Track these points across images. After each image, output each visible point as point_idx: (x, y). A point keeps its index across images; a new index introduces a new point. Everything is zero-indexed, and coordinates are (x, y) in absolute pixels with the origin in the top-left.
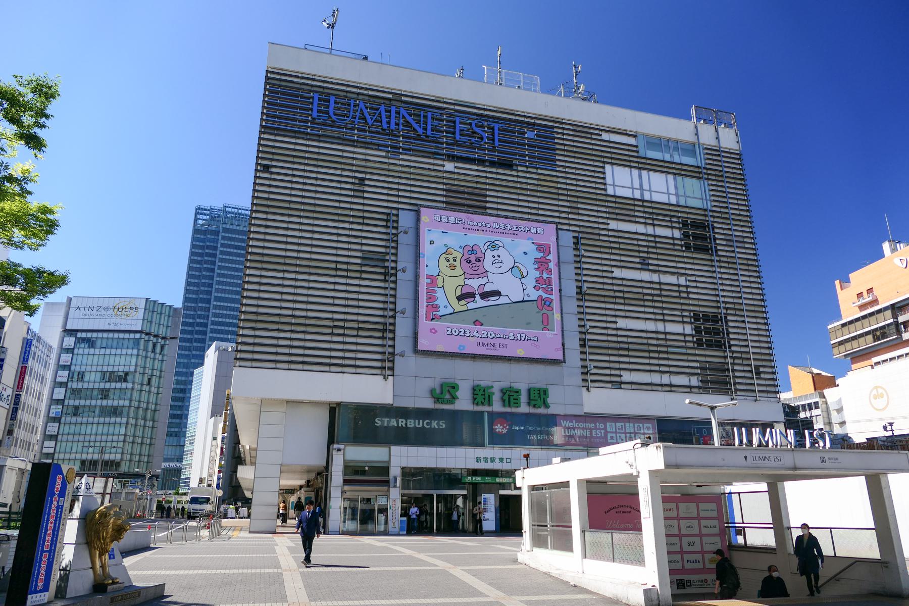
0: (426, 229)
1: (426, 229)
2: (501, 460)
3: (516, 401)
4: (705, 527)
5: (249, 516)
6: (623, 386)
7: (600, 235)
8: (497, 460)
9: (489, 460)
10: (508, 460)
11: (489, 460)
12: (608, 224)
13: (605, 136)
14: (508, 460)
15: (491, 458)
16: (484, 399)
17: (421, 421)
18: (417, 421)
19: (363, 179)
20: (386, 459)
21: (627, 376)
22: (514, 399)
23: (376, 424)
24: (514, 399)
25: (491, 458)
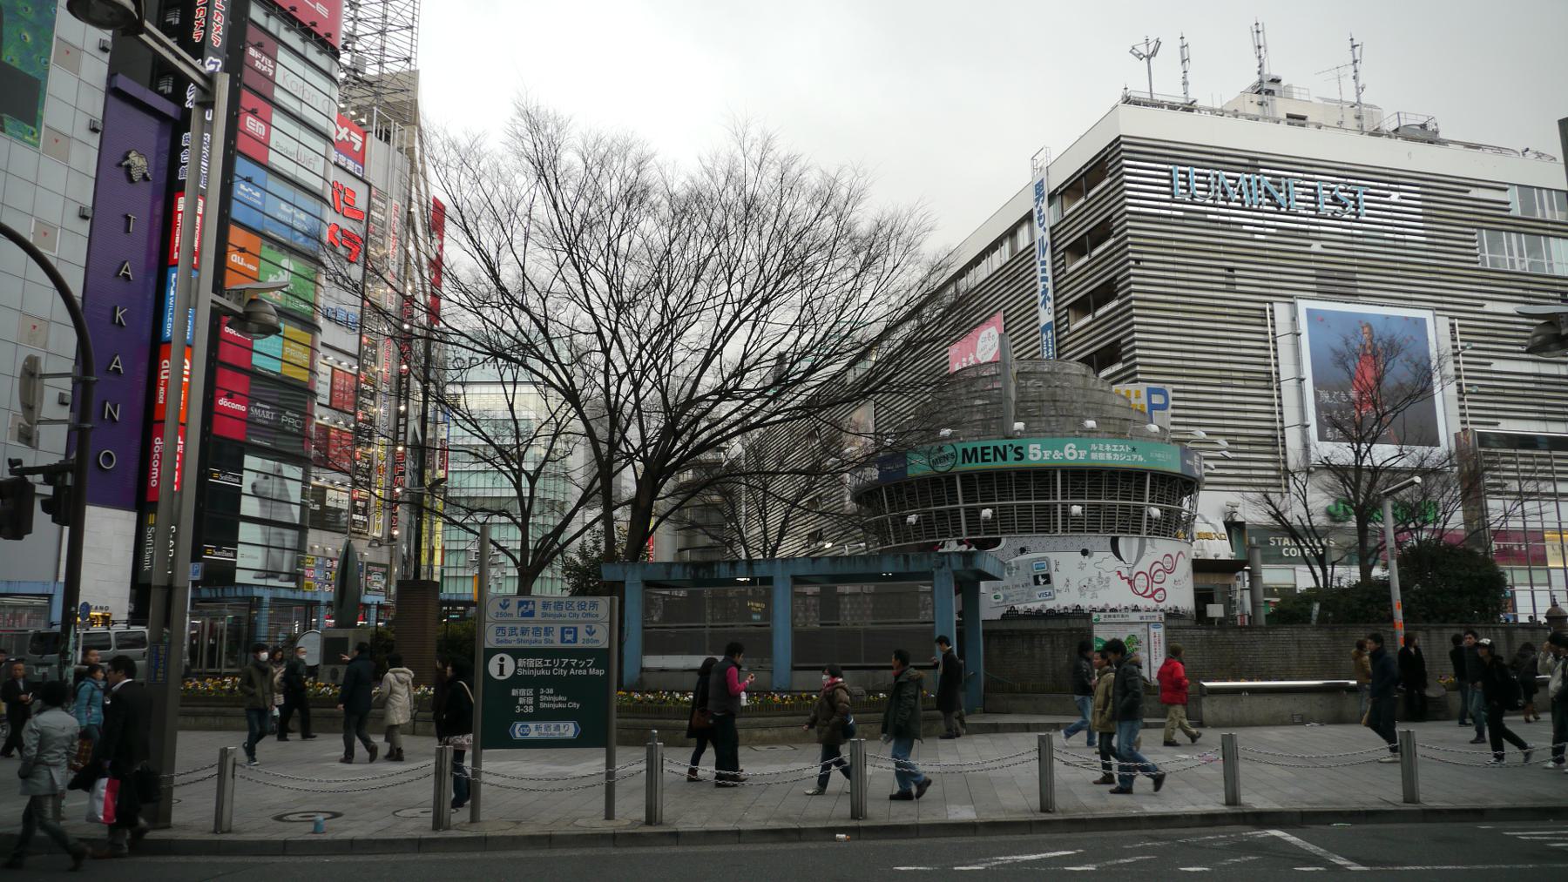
13: (1474, 193)
20: (1293, 582)
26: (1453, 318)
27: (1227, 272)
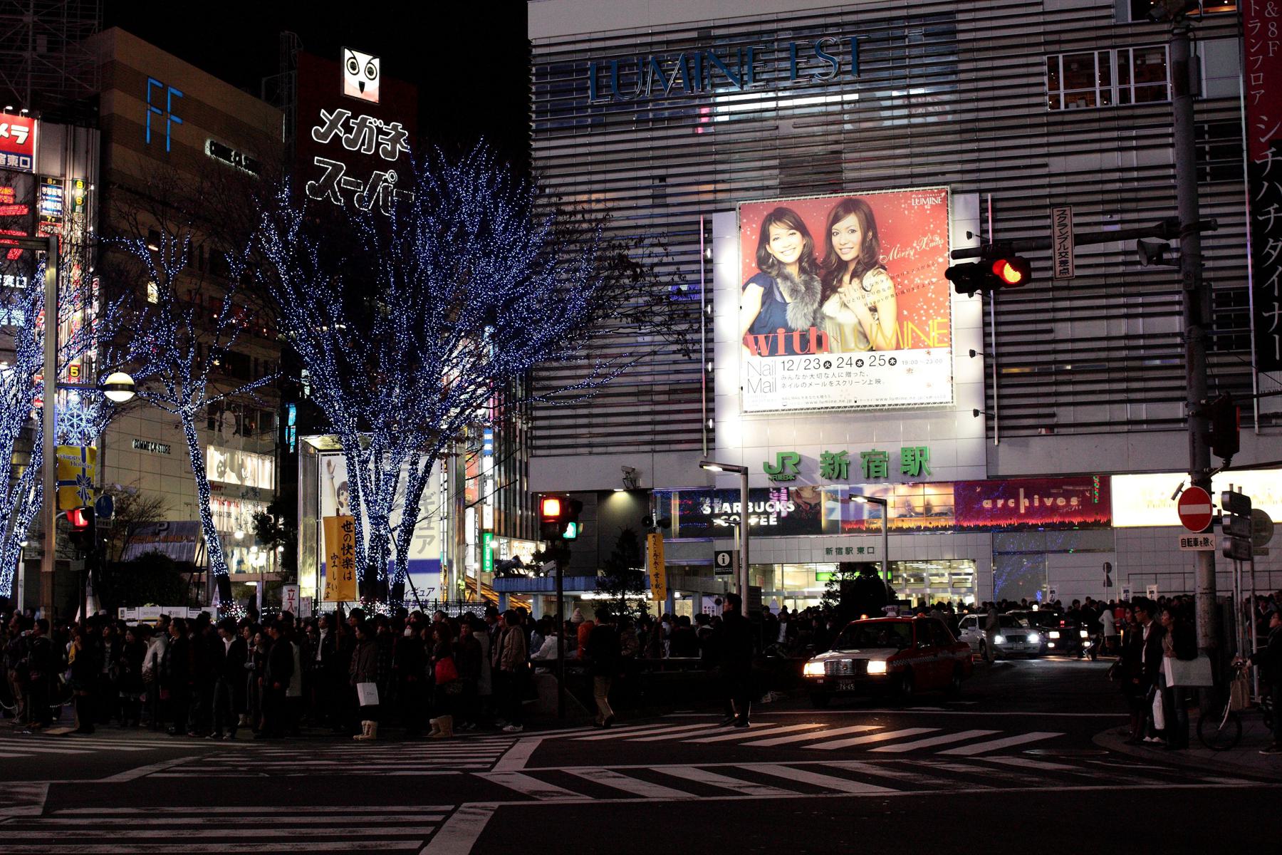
0: (316, 158)
1: (316, 158)
2: (861, 550)
3: (877, 469)
4: (941, 361)
5: (717, 554)
6: (478, 550)
7: (954, 112)
8: (855, 551)
9: (844, 551)
10: (871, 550)
11: (844, 551)
12: (1053, 415)
14: (871, 550)
15: (847, 548)
16: (833, 470)
17: (762, 504)
18: (756, 504)
19: (662, 178)
21: (1065, 415)
22: (876, 466)
23: (79, 648)
24: (876, 466)
25: (847, 548)
26: (980, 191)
27: (657, 182)
